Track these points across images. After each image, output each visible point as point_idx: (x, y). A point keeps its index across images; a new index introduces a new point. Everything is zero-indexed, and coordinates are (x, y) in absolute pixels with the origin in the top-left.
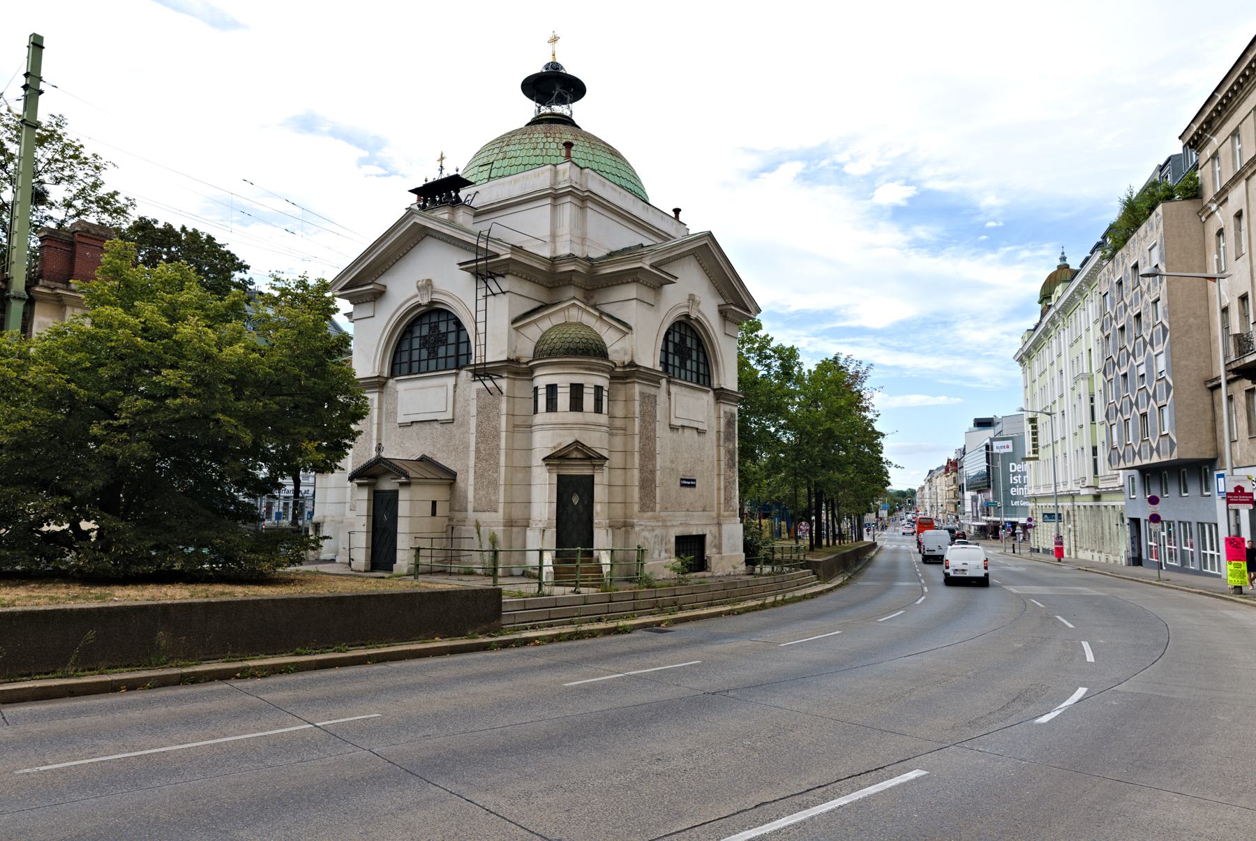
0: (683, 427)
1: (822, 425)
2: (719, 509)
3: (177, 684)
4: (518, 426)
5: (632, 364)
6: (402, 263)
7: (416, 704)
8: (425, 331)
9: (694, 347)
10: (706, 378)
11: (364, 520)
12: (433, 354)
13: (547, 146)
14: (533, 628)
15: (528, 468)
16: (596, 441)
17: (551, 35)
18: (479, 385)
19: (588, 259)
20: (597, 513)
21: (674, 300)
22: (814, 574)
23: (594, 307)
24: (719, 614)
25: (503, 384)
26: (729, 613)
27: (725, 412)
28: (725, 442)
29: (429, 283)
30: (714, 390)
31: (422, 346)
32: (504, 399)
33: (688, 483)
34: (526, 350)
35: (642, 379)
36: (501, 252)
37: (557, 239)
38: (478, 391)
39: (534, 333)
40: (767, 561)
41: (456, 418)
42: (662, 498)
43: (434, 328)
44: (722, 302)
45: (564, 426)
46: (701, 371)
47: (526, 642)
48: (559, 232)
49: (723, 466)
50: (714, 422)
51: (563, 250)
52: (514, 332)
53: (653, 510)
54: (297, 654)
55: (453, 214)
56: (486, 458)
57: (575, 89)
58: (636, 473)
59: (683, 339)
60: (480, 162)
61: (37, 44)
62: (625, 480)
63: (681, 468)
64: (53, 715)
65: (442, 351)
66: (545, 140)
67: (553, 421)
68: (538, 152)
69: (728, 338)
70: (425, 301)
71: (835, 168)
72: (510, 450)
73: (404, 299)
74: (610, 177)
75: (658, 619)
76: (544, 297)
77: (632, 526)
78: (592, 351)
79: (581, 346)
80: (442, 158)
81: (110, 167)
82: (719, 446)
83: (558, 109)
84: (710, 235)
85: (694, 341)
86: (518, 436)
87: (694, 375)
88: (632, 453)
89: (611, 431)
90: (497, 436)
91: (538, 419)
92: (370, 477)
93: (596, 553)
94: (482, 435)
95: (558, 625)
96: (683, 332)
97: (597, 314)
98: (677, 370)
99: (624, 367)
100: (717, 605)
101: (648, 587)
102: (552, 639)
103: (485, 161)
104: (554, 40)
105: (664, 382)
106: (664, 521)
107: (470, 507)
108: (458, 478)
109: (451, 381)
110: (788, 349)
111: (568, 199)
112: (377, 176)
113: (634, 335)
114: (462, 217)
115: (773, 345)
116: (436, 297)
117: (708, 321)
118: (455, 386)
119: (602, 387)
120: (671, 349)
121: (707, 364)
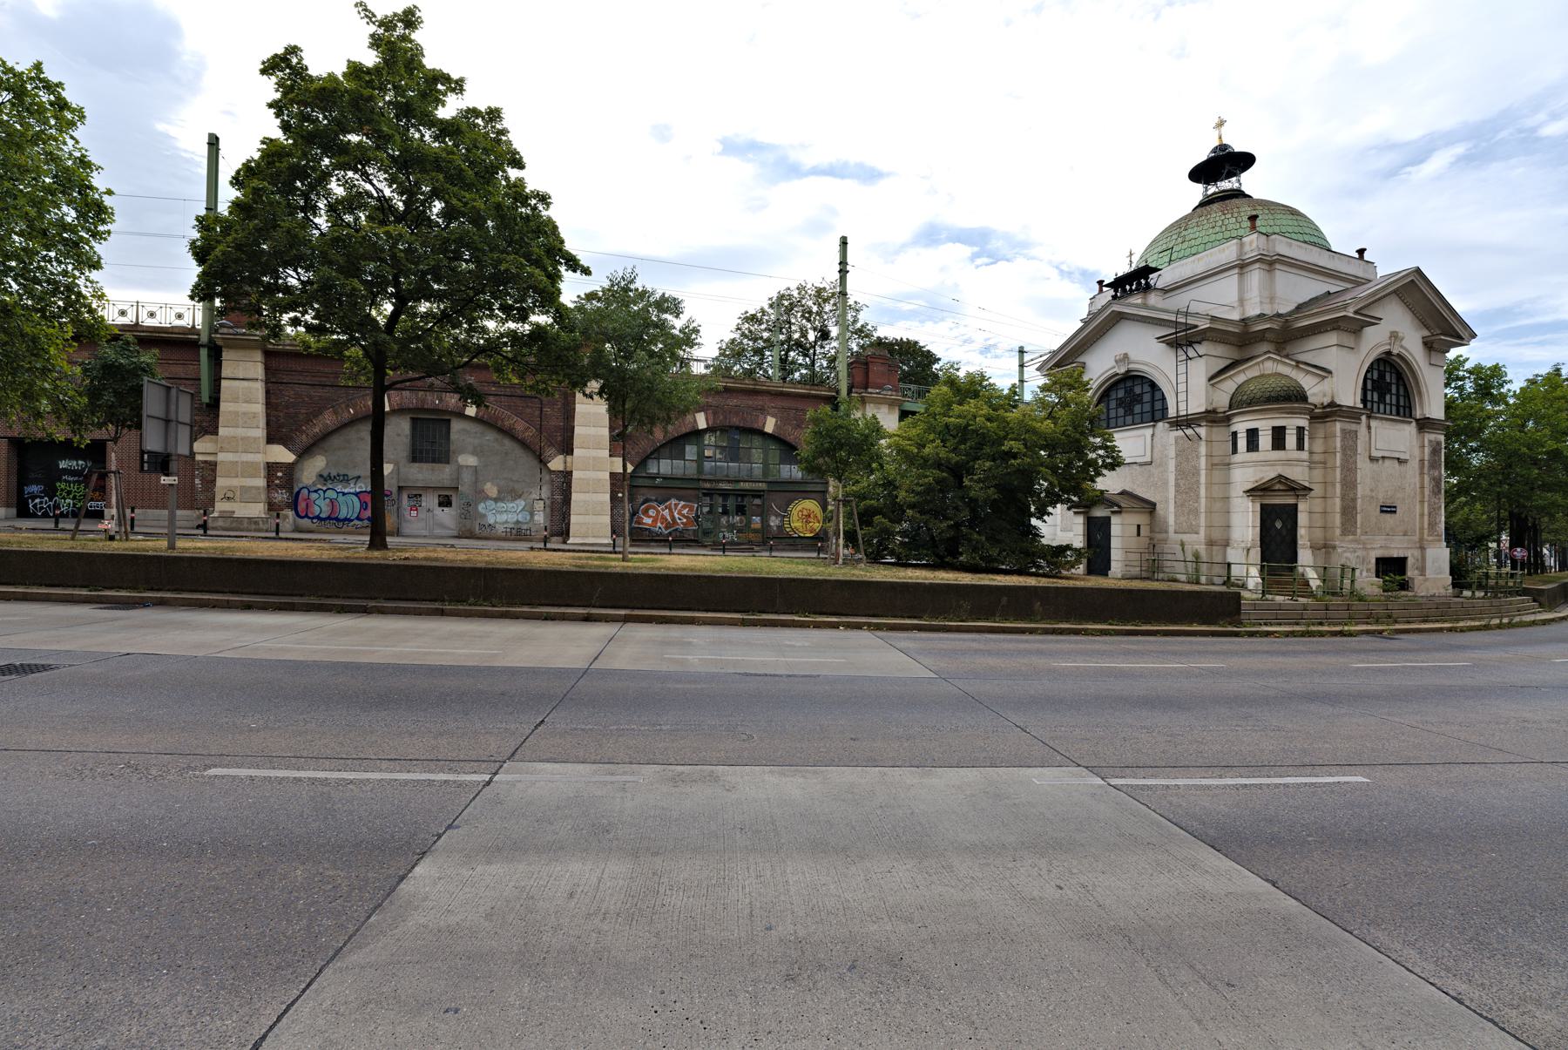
0: (1383, 458)
1: (1543, 447)
2: (1422, 534)
3: (1052, 633)
4: (1216, 465)
5: (1332, 404)
6: (1100, 342)
7: (1236, 662)
8: (1121, 394)
9: (1394, 381)
10: (1407, 410)
11: (1081, 538)
12: (1129, 411)
13: (1226, 222)
14: (1266, 624)
15: (1227, 499)
16: (1298, 474)
17: (1217, 120)
18: (1180, 433)
19: (1279, 315)
20: (1301, 536)
21: (1374, 341)
22: (1534, 601)
23: (1287, 356)
24: (1441, 630)
25: (1202, 431)
26: (1450, 630)
27: (1430, 441)
28: (1429, 471)
29: (1126, 356)
30: (1417, 420)
31: (1119, 406)
32: (1203, 443)
33: (1388, 509)
34: (1222, 400)
35: (1343, 417)
36: (1199, 324)
37: (1245, 303)
38: (1177, 439)
39: (1229, 386)
40: (1480, 587)
41: (1155, 459)
42: (1362, 525)
43: (1129, 391)
44: (1426, 333)
45: (1266, 463)
46: (1402, 403)
47: (1268, 634)
48: (1247, 296)
49: (1427, 492)
50: (1417, 452)
51: (1253, 311)
52: (1210, 388)
53: (1354, 534)
54: (1110, 624)
55: (1145, 298)
56: (1187, 490)
57: (1245, 161)
58: (1338, 501)
59: (1382, 376)
60: (1160, 249)
61: (844, 242)
62: (1325, 508)
63: (1381, 496)
64: (1011, 641)
65: (1137, 409)
66: (1223, 217)
67: (1254, 459)
68: (1217, 229)
69: (1433, 368)
70: (1122, 370)
71: (1523, 135)
72: (1209, 484)
73: (1102, 372)
74: (1293, 236)
75: (1380, 628)
76: (1234, 354)
77: (1334, 547)
78: (1293, 397)
79: (1282, 394)
80: (1131, 254)
81: (864, 308)
82: (1422, 474)
83: (1225, 185)
84: (1418, 271)
85: (1394, 375)
86: (1216, 473)
87: (1394, 408)
88: (1333, 484)
89: (1312, 464)
90: (1196, 472)
91: (1237, 458)
92: (1085, 507)
93: (1300, 570)
94: (1180, 472)
95: (1285, 624)
96: (1382, 368)
97: (1294, 363)
98: (1375, 405)
99: (1324, 407)
100: (1432, 621)
101: (1360, 600)
102: (1287, 634)
103: (1164, 247)
104: (1221, 124)
105: (1364, 418)
106: (1364, 544)
107: (1171, 529)
108: (1158, 507)
109: (1149, 432)
110: (1489, 369)
111: (1257, 265)
112: (987, 265)
113: (1335, 379)
114: (1153, 299)
115: (1468, 366)
116: (1132, 366)
117: (1410, 354)
118: (1153, 435)
119: (1303, 428)
120: (1369, 386)
121: (1407, 396)
